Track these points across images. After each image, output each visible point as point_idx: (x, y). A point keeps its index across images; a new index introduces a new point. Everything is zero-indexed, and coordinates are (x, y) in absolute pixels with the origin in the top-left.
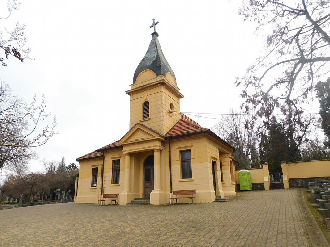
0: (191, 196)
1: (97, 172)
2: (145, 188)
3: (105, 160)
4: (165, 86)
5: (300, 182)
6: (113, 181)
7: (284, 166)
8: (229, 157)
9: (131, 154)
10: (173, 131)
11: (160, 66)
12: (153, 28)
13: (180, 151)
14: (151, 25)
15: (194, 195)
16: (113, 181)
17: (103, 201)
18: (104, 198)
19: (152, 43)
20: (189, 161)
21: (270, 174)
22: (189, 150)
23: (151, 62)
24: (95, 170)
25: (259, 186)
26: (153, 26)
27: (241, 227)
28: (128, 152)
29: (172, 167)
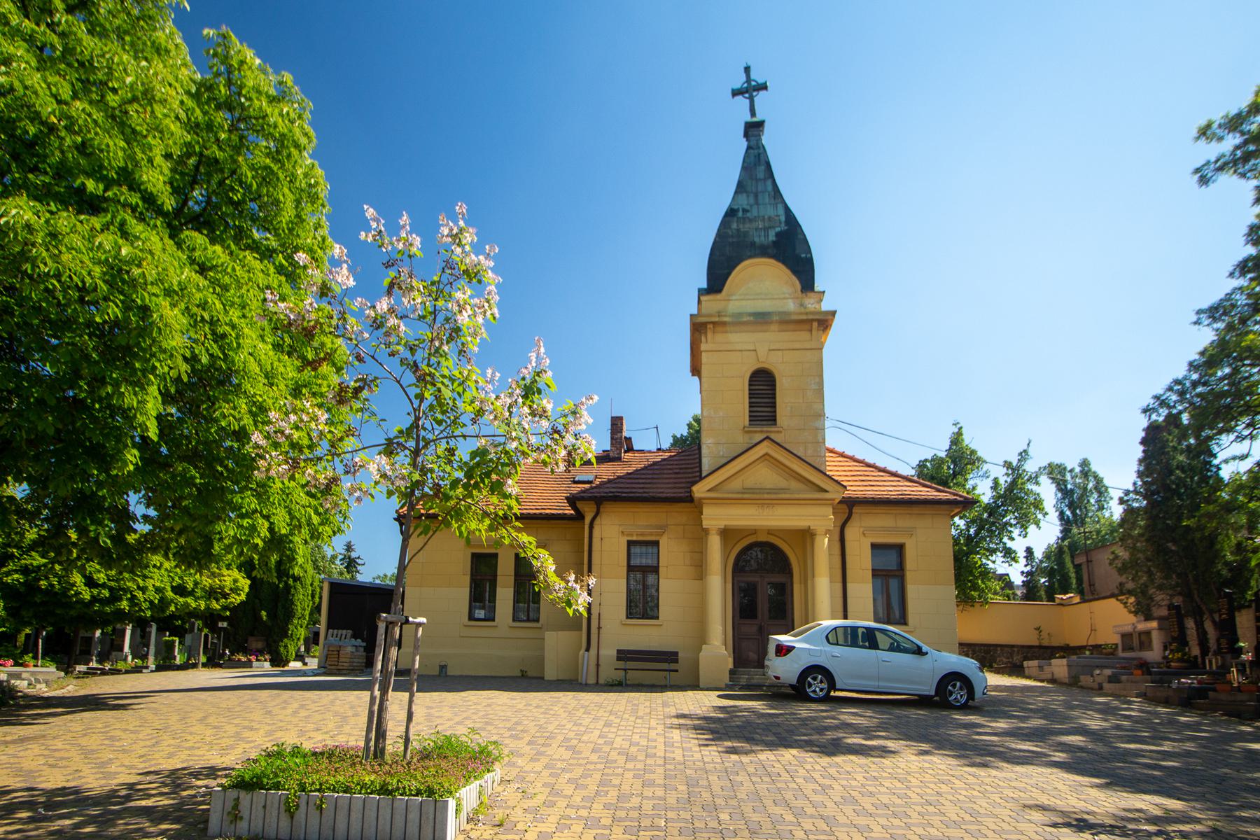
28: (722, 524)
29: (849, 586)
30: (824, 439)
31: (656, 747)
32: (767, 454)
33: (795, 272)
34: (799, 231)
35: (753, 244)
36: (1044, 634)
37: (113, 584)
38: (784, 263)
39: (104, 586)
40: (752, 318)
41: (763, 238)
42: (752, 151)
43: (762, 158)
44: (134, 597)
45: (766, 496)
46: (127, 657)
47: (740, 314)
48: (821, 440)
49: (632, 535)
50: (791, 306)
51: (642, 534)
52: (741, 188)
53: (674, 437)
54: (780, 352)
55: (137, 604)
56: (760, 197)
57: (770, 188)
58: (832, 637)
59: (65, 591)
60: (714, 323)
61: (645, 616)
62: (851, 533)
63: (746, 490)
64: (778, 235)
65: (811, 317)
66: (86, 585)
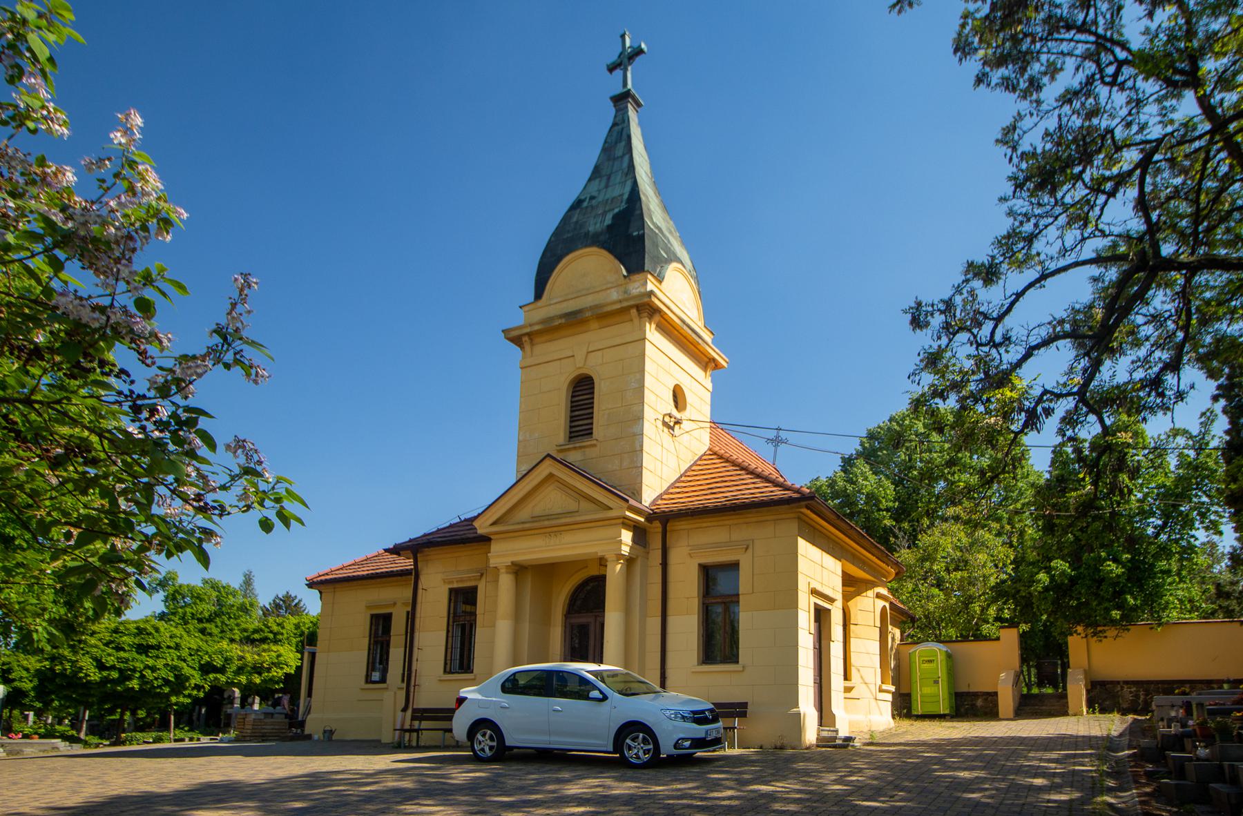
1: (387, 630)
3: (420, 586)
4: (657, 318)
6: (449, 662)
7: (1077, 645)
8: (878, 596)
9: (519, 570)
11: (641, 238)
12: (618, 73)
13: (700, 565)
14: (613, 58)
16: (449, 662)
17: (411, 731)
18: (416, 723)
21: (1024, 660)
22: (734, 566)
24: (381, 624)
25: (979, 702)
28: (508, 561)
29: (672, 620)
30: (642, 446)
32: (551, 476)
34: (638, 205)
35: (587, 234)
37: (122, 665)
38: (610, 251)
39: (113, 668)
40: (563, 321)
44: (143, 676)
45: (546, 523)
47: (551, 319)
48: (638, 448)
49: (452, 582)
51: (461, 580)
52: (596, 173)
54: (600, 353)
55: (147, 683)
56: (612, 178)
57: (625, 164)
58: (511, 686)
59: (75, 674)
60: (528, 334)
62: (676, 556)
63: (535, 519)
64: (615, 217)
65: (625, 304)
66: (97, 667)
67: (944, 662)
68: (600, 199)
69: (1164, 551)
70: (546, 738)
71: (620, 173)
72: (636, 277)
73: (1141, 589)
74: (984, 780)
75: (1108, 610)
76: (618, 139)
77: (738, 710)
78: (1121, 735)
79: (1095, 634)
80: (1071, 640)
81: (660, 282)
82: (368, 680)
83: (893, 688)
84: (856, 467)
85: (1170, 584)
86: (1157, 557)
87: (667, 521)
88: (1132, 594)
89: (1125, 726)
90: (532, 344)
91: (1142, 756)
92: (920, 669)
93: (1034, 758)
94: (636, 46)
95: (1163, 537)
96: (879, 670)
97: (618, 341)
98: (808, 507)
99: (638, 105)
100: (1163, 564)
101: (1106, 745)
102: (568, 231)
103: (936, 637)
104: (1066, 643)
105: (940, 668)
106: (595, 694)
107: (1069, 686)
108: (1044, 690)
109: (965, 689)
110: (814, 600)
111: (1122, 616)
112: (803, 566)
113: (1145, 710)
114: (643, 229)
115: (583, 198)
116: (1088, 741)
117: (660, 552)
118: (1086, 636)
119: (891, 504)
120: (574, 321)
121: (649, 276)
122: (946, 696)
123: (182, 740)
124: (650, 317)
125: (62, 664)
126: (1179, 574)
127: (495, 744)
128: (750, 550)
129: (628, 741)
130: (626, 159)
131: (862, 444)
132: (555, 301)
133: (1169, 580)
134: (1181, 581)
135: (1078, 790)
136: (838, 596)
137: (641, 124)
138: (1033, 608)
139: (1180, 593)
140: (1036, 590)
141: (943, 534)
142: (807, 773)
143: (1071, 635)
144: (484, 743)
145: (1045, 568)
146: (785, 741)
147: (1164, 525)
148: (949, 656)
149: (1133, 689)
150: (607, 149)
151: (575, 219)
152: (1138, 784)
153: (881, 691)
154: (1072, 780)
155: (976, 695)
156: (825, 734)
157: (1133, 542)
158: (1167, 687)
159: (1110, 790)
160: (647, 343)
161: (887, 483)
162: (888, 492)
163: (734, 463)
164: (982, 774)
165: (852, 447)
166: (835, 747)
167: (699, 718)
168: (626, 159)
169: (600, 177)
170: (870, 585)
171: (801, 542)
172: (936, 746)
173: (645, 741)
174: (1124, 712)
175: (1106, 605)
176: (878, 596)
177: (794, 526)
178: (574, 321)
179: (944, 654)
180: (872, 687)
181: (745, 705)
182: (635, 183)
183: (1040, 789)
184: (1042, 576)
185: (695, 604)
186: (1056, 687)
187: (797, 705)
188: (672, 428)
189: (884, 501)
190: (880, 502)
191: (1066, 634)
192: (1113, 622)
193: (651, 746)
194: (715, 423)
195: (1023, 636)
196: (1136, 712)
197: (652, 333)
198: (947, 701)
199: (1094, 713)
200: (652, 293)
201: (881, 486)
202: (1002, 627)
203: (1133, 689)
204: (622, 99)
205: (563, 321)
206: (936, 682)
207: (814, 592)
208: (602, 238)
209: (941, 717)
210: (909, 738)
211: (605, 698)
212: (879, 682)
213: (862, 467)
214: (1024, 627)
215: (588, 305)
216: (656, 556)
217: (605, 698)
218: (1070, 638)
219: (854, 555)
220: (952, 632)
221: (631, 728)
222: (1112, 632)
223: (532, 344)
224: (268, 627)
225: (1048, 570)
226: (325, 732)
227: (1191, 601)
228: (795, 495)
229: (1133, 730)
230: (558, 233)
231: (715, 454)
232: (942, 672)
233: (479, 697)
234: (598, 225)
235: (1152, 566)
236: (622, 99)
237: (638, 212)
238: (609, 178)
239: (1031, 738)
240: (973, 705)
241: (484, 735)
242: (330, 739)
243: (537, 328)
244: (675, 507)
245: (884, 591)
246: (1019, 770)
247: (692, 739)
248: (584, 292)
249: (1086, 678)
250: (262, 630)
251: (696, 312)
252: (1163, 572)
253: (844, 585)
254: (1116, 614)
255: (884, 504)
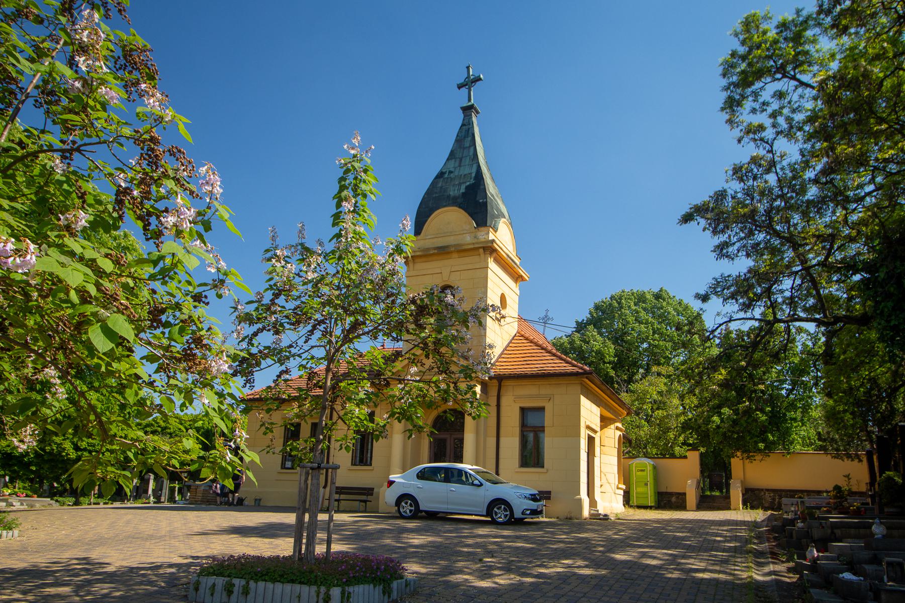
0: (364, 497)
2: (460, 482)
4: (494, 255)
5: (768, 497)
7: (736, 464)
8: (617, 428)
10: (504, 360)
11: (485, 205)
12: (464, 90)
14: (462, 81)
15: (369, 498)
19: (463, 134)
20: (539, 430)
21: (702, 472)
22: (542, 409)
23: (463, 190)
25: (674, 499)
26: (466, 85)
27: (587, 599)
29: (502, 440)
31: (688, 594)
33: (472, 215)
34: (482, 183)
35: (449, 196)
36: (853, 481)
37: (91, 448)
39: (85, 449)
40: (436, 251)
41: (456, 191)
42: (464, 127)
43: (470, 131)
46: (150, 497)
47: (428, 249)
50: (468, 239)
52: (452, 156)
53: (577, 322)
56: (463, 160)
59: (60, 453)
61: (366, 464)
62: (504, 401)
64: (467, 188)
66: (74, 449)
67: (652, 471)
68: (456, 173)
69: (792, 406)
70: (446, 506)
71: (468, 158)
72: (482, 229)
73: (778, 430)
74: (690, 537)
75: (756, 443)
76: (465, 136)
77: (545, 495)
78: (763, 521)
79: (748, 458)
80: (733, 461)
81: (496, 232)
82: (283, 467)
83: (624, 487)
84: (589, 331)
85: (796, 427)
86: (788, 409)
87: (502, 380)
88: (771, 433)
89: (765, 517)
90: (414, 263)
91: (773, 530)
92: (635, 475)
93: (713, 529)
94: (477, 75)
95: (792, 396)
96: (617, 475)
97: (470, 267)
98: (587, 378)
99: (477, 112)
100: (792, 414)
101: (755, 525)
102: (436, 193)
103: (644, 454)
104: (730, 464)
105: (649, 476)
106: (476, 482)
107: (731, 491)
108: (714, 493)
109: (664, 490)
110: (588, 432)
111: (766, 448)
112: (583, 412)
113: (779, 508)
114: (486, 198)
115: (444, 171)
116: (743, 523)
117: (495, 398)
118: (743, 458)
119: (612, 359)
120: (443, 251)
121: (491, 229)
122: (653, 494)
123: (98, 504)
124: (491, 254)
125: (50, 445)
126: (802, 420)
127: (413, 508)
128: (551, 401)
129: (495, 509)
130: (472, 149)
131: (591, 313)
132: (429, 237)
133: (795, 425)
134: (803, 425)
135: (739, 542)
136: (598, 429)
137: (478, 125)
138: (709, 439)
139: (802, 433)
140: (711, 427)
141: (650, 385)
142: (484, 566)
143: (733, 457)
144: (406, 508)
145: (717, 413)
146: (572, 515)
147: (793, 389)
148: (655, 468)
149: (772, 495)
150: (459, 141)
151: (440, 185)
152: (769, 541)
153: (618, 488)
154: (735, 538)
155: (671, 494)
156: (592, 512)
157: (773, 400)
158: (791, 493)
159: (754, 544)
160: (489, 270)
161: (609, 343)
162: (610, 350)
163: (537, 344)
164: (688, 534)
165: (584, 316)
166: (600, 519)
167: (534, 498)
168: (472, 149)
169: (455, 158)
170: (614, 421)
171: (582, 398)
172: (658, 521)
173: (505, 510)
174: (765, 509)
175: (755, 439)
176: (617, 428)
177: (578, 388)
178: (443, 251)
179: (651, 466)
180: (613, 486)
181: (549, 493)
182: (479, 167)
183: (720, 541)
184: (716, 419)
185: (517, 430)
186: (721, 491)
187: (579, 494)
188: (499, 321)
189: (607, 356)
190: (606, 357)
191: (733, 456)
192: (760, 451)
193: (508, 513)
194: (520, 319)
195: (701, 455)
196: (773, 509)
197: (492, 265)
198: (653, 497)
199: (747, 509)
200: (493, 241)
201: (606, 346)
202: (688, 450)
203: (772, 495)
204: (468, 110)
205: (436, 251)
206: (646, 484)
207: (588, 427)
208: (459, 200)
209: (651, 508)
210: (637, 517)
211: (481, 485)
212: (617, 483)
213: (592, 331)
214: (702, 450)
215: (453, 243)
216: (493, 401)
217: (481, 485)
218: (732, 460)
219: (606, 404)
220: (654, 451)
221: (498, 502)
222: (759, 457)
223: (414, 263)
224: (157, 423)
225: (720, 414)
226: (256, 500)
227: (809, 438)
228: (580, 371)
229: (769, 519)
230: (429, 192)
231: (522, 336)
232: (650, 479)
233: (403, 481)
234: (456, 191)
235: (785, 415)
236: (468, 110)
237: (482, 187)
238: (461, 160)
239: (710, 521)
240: (670, 501)
241: (406, 503)
242: (259, 505)
243: (418, 254)
244: (507, 372)
245: (619, 425)
246: (707, 534)
247: (531, 510)
248: (449, 234)
249: (742, 486)
250: (152, 425)
251: (512, 246)
252: (792, 419)
253: (601, 422)
254: (761, 445)
255: (607, 359)
